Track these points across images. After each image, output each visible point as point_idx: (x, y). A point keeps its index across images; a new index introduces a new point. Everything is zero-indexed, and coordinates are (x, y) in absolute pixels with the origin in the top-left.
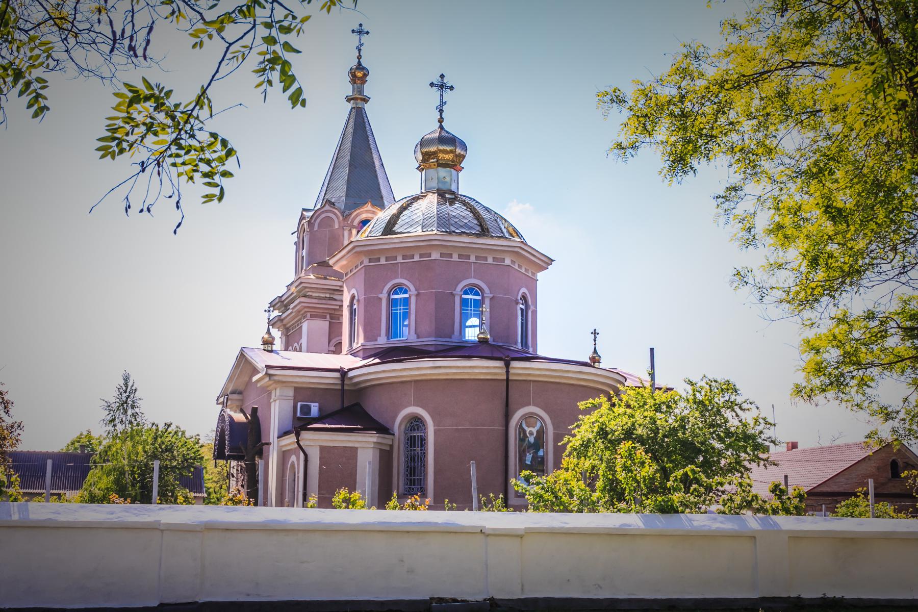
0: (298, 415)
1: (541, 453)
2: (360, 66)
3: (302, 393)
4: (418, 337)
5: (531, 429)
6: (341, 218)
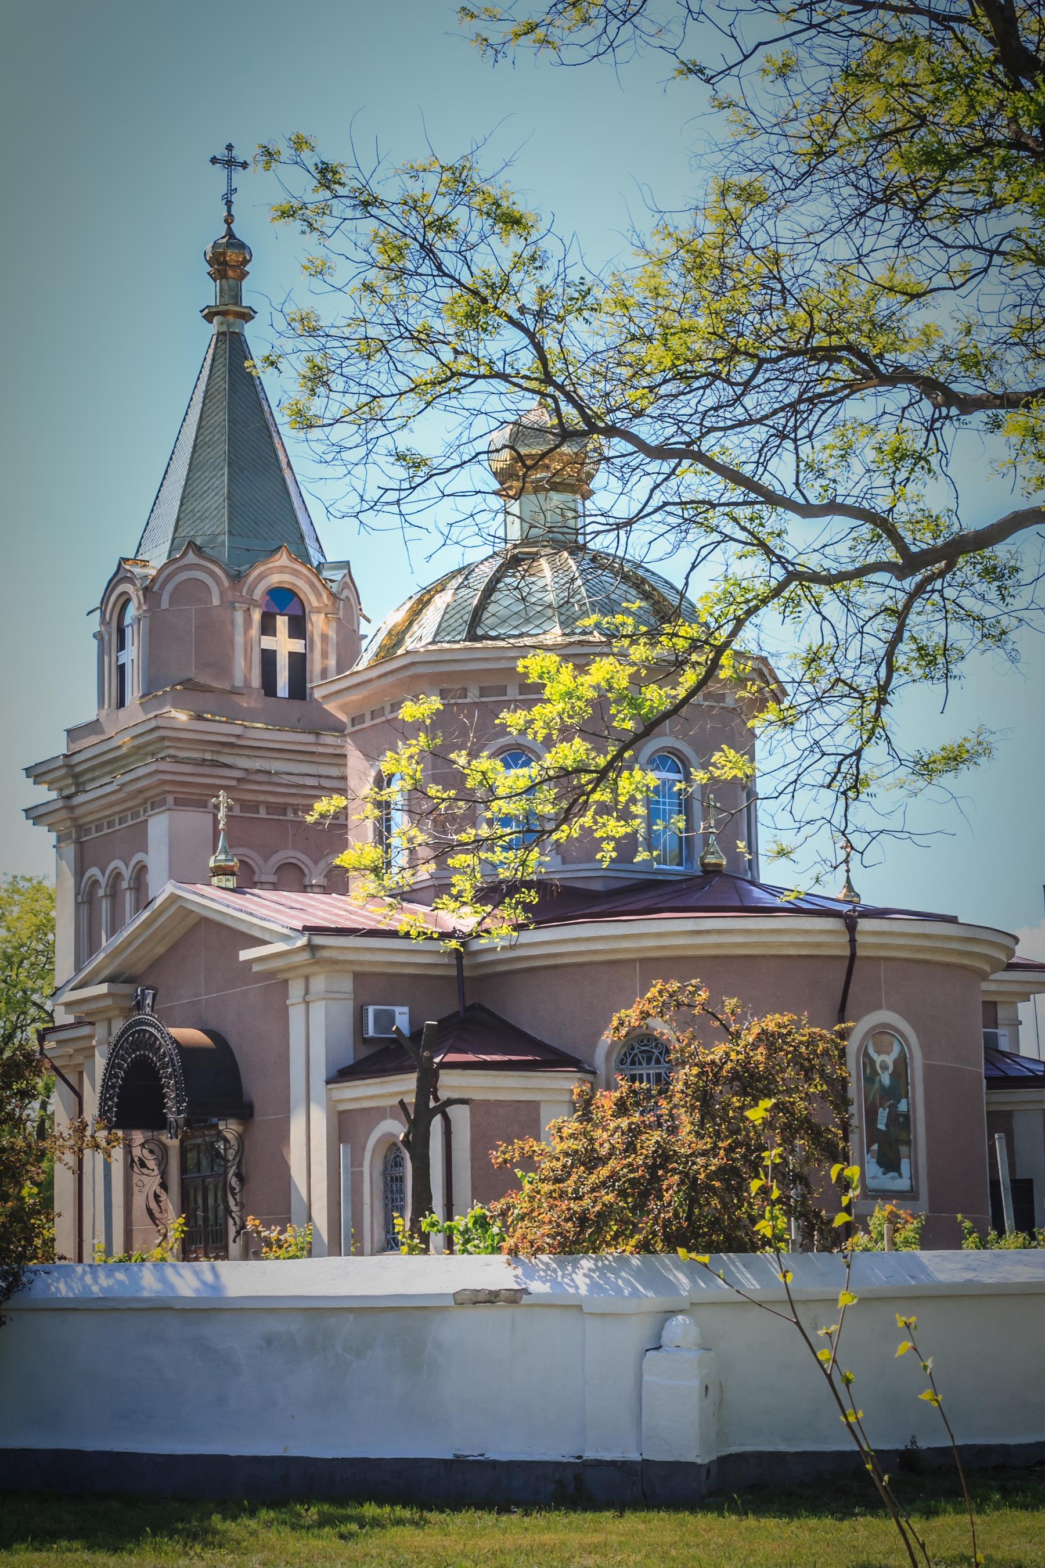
0: (371, 1032)
1: (903, 1106)
2: (232, 241)
3: (372, 986)
4: (564, 863)
5: (883, 1057)
6: (226, 583)
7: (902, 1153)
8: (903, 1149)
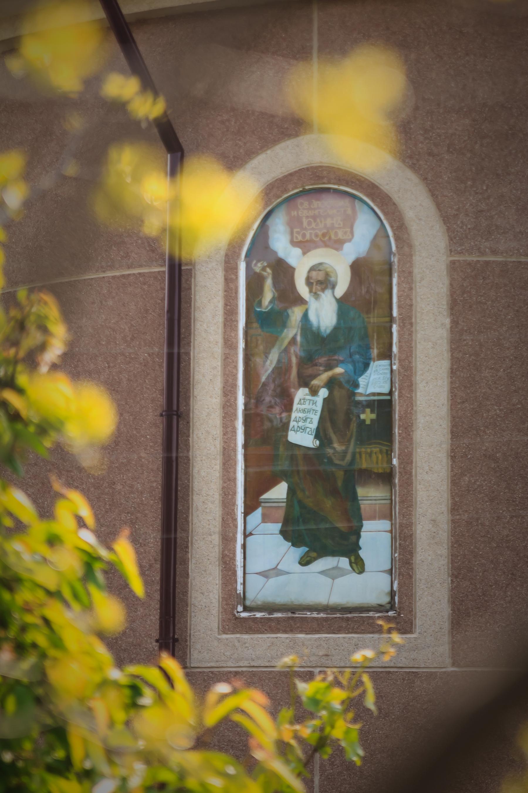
5: (318, 256)
7: (364, 505)
8: (370, 495)
